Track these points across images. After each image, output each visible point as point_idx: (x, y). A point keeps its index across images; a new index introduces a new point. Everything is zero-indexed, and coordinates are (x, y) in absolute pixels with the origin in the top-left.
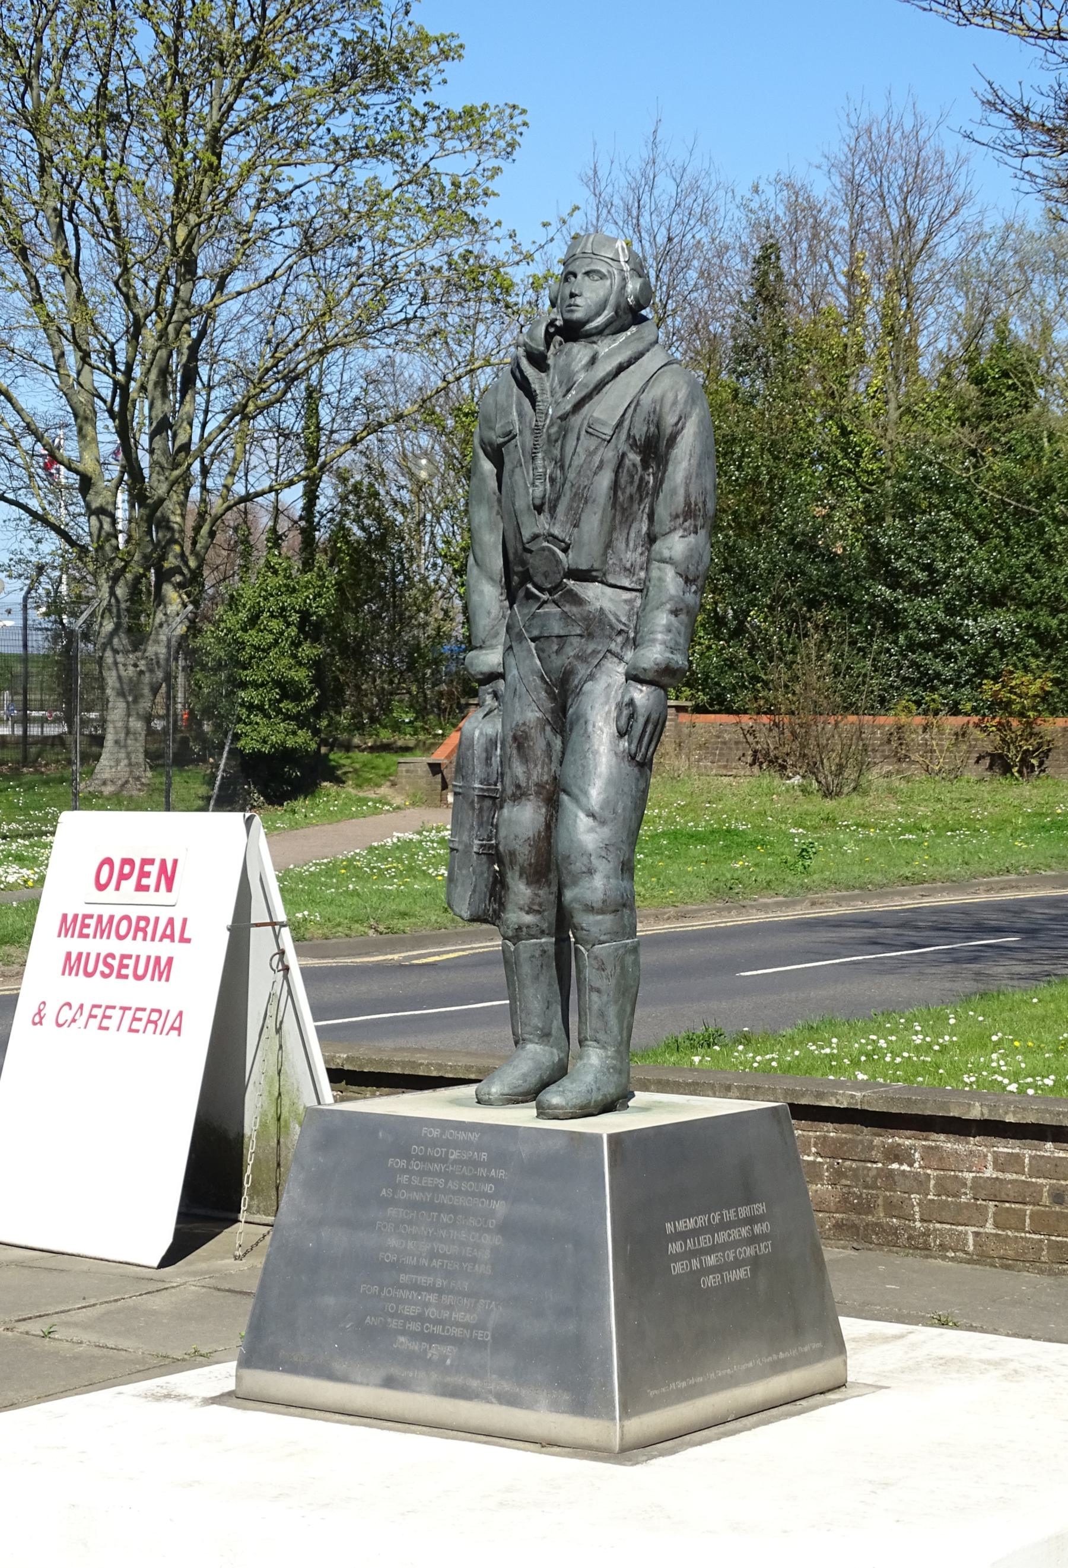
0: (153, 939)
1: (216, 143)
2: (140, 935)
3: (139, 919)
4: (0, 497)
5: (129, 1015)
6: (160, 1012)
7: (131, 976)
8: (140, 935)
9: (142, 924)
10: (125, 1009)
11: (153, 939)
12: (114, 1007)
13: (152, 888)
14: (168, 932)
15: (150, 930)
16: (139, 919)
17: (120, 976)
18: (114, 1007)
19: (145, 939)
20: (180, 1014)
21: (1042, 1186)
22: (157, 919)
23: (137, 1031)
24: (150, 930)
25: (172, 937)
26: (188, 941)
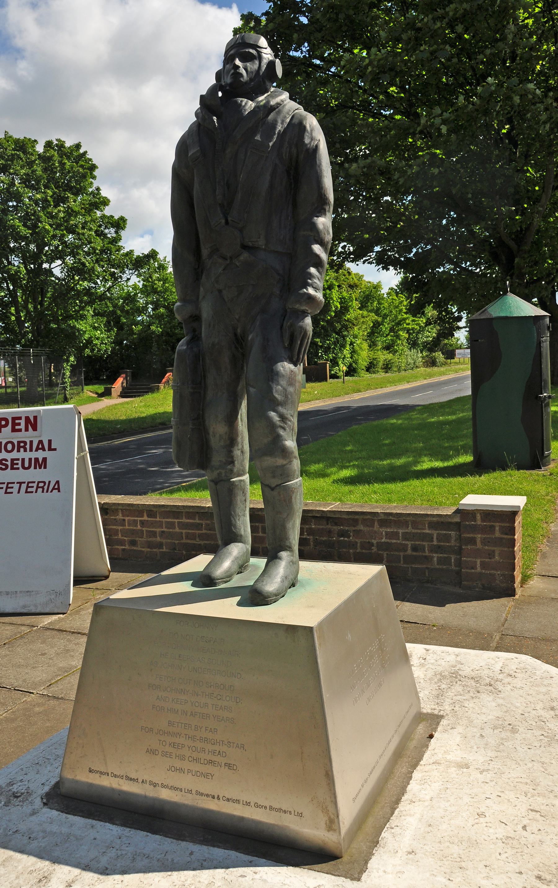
0: (47, 492)
1: (427, 806)
2: (22, 450)
3: (19, 443)
4: (0, 687)
5: (24, 486)
6: (44, 483)
7: (21, 468)
8: (22, 450)
9: (22, 444)
10: (20, 483)
11: (47, 492)
12: (14, 483)
13: (23, 429)
14: (40, 447)
15: (46, 487)
16: (19, 443)
17: (12, 468)
18: (14, 483)
19: (43, 492)
20: (58, 482)
21: (404, 563)
22: (50, 482)
23: (32, 492)
24: (46, 487)
25: (43, 449)
26: (55, 450)
